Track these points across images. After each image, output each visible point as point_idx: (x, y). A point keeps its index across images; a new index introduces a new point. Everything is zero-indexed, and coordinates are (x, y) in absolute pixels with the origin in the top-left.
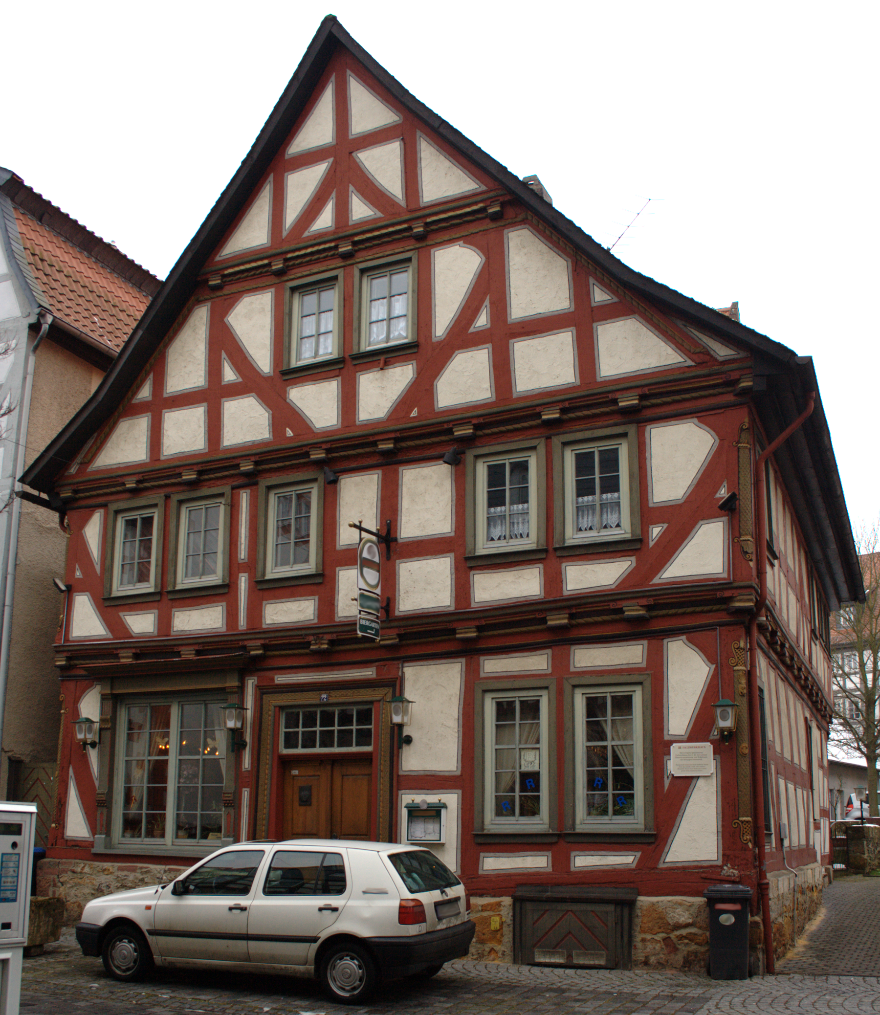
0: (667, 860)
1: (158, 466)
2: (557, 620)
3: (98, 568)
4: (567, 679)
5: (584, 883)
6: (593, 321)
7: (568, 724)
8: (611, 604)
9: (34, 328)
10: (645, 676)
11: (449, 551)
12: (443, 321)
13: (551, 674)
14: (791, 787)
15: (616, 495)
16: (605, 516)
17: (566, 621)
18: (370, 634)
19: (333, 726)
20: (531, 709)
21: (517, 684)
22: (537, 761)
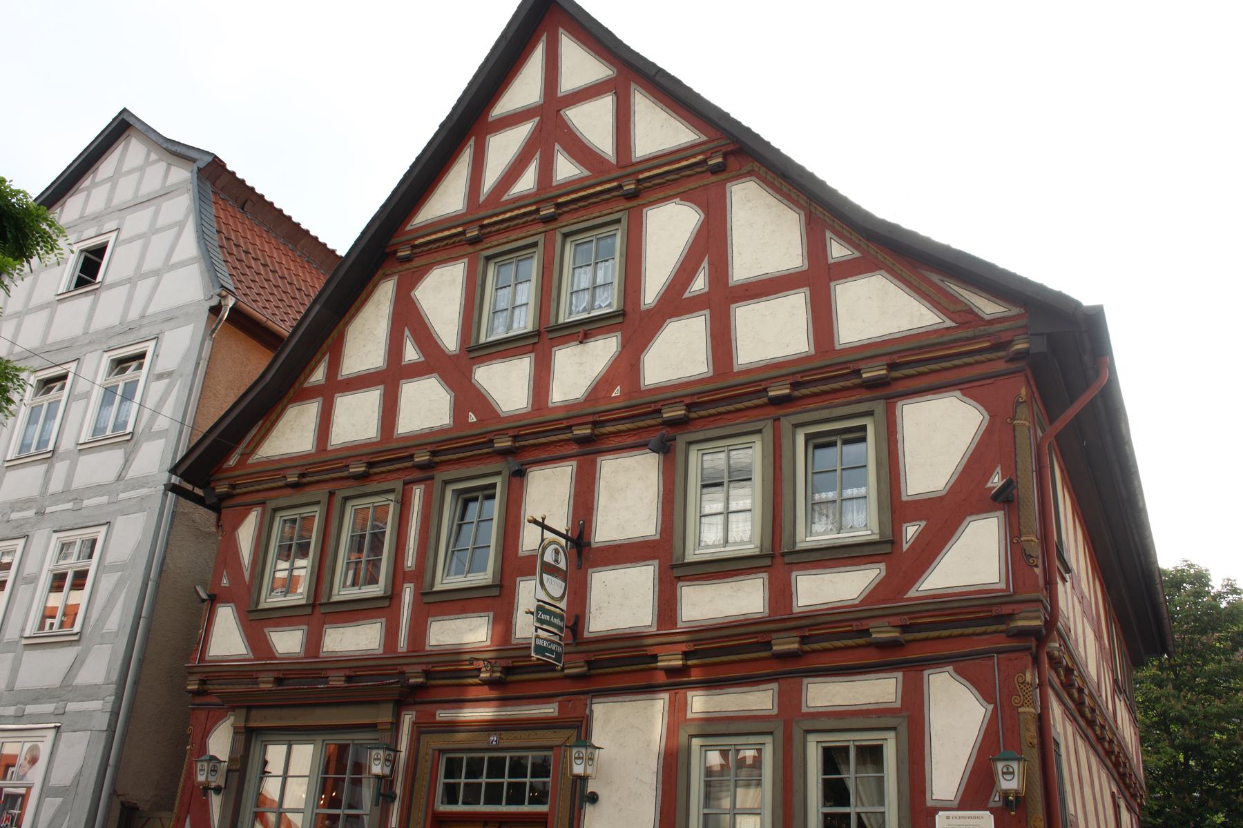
1: (324, 457)
2: (785, 644)
3: (247, 575)
6: (831, 280)
8: (855, 623)
9: (215, 311)
11: (653, 558)
12: (652, 288)
18: (549, 658)
19: (503, 777)
21: (733, 728)
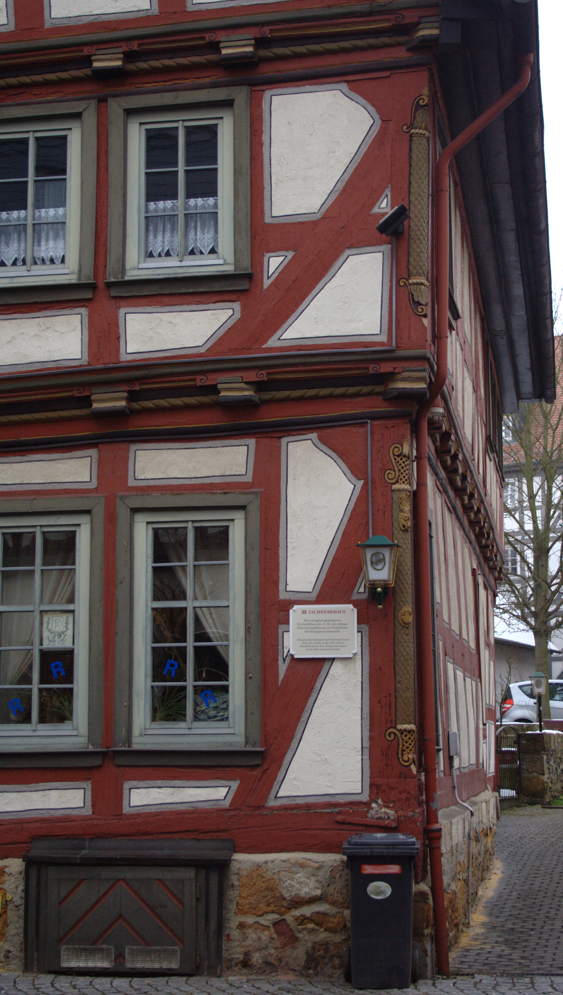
0: (280, 794)
4: (122, 498)
5: (146, 834)
7: (122, 572)
8: (199, 377)
10: (251, 497)
13: (96, 490)
14: (460, 674)
15: (211, 201)
16: (192, 235)
17: (123, 403)
20: (62, 548)
21: (39, 505)
22: (70, 633)
